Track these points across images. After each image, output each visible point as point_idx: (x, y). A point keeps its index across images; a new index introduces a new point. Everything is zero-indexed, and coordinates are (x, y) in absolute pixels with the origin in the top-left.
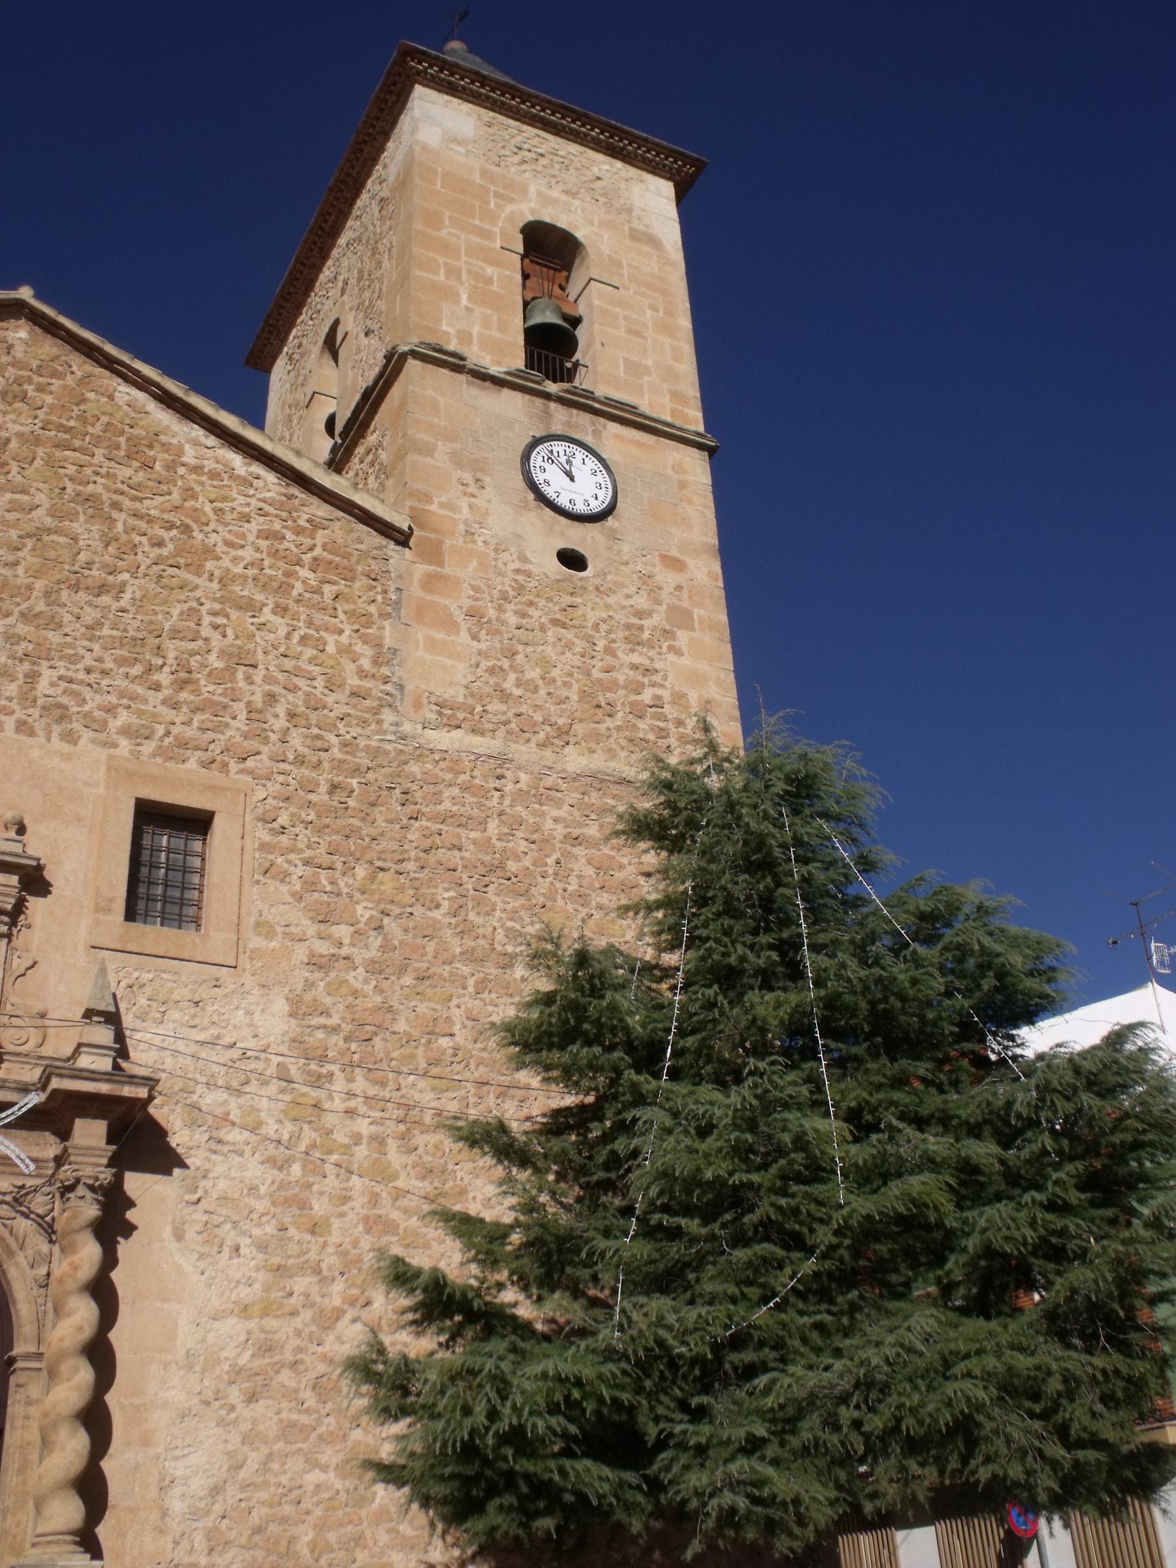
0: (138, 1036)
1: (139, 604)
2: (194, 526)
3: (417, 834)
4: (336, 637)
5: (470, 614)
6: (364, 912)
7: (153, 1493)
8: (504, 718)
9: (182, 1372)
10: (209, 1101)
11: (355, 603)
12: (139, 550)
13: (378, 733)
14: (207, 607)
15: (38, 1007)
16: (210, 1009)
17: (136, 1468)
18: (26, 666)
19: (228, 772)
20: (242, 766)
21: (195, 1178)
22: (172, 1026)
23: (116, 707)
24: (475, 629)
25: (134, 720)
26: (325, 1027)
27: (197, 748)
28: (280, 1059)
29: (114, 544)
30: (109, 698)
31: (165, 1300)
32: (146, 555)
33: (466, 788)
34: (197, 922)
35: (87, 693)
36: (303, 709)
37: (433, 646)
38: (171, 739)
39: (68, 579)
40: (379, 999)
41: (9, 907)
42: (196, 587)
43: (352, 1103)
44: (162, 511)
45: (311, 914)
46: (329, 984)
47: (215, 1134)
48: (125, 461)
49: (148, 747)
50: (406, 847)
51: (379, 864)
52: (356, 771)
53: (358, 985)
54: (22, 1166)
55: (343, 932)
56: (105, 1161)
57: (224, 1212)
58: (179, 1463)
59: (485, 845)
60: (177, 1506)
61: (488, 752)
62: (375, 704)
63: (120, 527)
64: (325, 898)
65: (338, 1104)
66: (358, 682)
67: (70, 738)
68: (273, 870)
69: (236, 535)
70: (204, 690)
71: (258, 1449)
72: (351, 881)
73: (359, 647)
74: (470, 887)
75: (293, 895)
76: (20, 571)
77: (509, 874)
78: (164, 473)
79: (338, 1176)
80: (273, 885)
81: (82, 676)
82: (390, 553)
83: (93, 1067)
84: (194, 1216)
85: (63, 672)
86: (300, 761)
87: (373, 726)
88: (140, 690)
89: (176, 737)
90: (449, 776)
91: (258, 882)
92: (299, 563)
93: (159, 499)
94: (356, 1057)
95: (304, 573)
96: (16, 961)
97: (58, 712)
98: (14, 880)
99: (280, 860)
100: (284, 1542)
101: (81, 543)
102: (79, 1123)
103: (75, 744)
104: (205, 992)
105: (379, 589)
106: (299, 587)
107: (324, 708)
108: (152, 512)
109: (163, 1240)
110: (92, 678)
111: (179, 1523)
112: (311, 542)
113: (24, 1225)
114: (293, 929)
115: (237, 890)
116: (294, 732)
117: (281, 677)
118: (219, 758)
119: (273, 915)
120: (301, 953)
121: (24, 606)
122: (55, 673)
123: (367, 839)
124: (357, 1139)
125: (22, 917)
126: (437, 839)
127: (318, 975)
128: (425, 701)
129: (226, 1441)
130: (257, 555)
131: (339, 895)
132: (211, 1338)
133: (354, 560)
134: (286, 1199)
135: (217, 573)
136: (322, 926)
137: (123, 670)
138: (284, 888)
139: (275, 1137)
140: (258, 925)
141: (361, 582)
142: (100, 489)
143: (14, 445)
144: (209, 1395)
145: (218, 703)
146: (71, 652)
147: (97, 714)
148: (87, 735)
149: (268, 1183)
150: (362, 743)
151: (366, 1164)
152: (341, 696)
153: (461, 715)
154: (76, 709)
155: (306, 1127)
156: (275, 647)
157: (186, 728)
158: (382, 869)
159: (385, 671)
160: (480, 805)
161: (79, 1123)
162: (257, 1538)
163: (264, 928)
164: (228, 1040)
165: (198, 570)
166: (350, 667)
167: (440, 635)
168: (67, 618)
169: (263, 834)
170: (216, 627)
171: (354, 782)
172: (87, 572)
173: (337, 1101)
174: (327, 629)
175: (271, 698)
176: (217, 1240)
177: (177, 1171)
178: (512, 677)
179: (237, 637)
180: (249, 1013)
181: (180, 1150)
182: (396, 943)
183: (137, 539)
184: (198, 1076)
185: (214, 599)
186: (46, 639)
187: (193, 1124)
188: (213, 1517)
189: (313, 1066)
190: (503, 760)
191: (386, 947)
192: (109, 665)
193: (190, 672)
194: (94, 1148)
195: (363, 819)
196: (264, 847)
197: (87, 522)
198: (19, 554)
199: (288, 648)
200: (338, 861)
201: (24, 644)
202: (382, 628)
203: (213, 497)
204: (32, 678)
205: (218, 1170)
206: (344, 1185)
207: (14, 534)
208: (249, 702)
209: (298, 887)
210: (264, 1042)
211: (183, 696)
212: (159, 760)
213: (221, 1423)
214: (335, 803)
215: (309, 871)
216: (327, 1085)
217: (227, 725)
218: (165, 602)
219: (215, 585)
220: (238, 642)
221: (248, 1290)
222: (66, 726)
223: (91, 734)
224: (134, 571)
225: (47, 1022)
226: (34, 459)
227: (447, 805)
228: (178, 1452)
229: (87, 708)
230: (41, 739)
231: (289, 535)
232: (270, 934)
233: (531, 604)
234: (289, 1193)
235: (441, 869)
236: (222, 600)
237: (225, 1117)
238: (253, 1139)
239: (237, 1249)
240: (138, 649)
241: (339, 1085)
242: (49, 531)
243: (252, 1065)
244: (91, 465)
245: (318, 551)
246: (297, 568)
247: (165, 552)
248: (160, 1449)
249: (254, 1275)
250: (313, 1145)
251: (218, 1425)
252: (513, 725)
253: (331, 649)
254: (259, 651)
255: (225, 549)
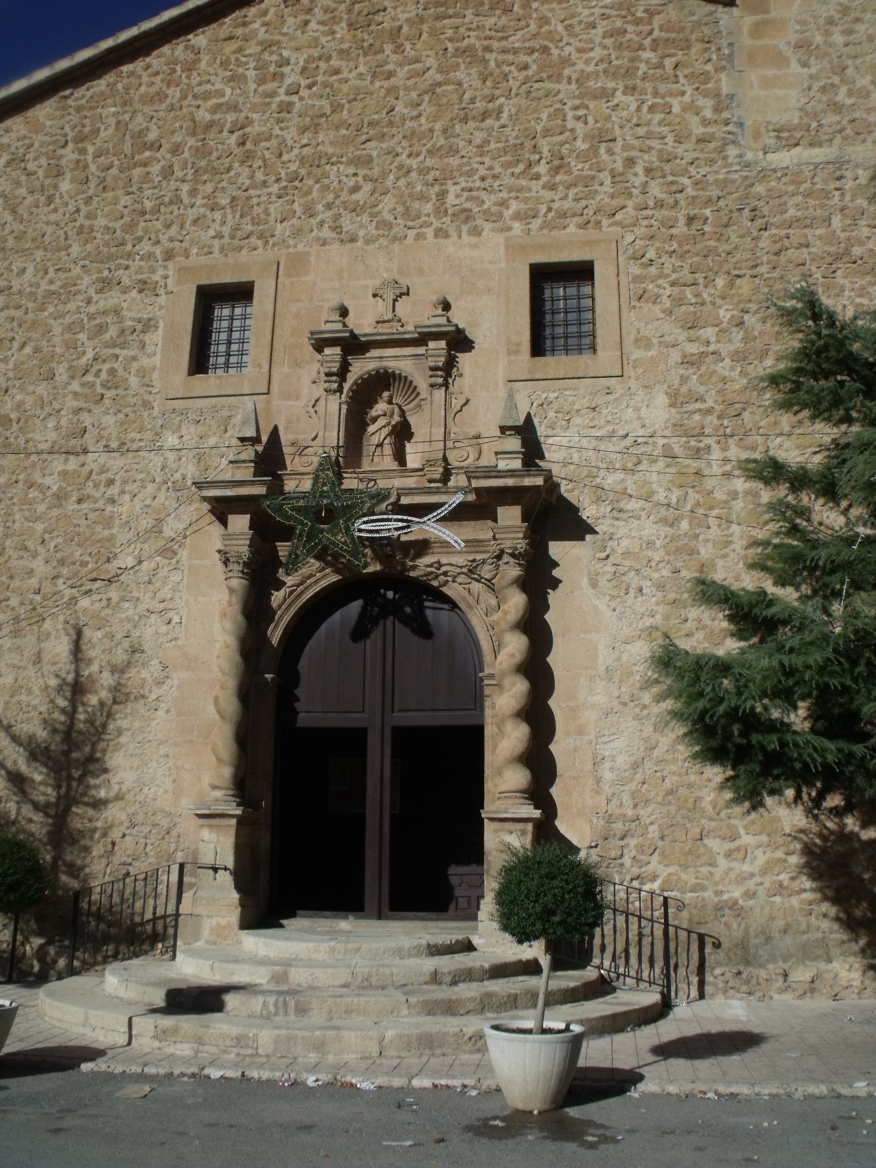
0: (550, 441)
1: (514, 118)
2: (551, 45)
3: (767, 242)
4: (680, 98)
5: (798, 46)
6: (725, 313)
7: (589, 766)
8: (839, 127)
9: (604, 683)
10: (609, 481)
11: (692, 66)
12: (510, 78)
13: (724, 167)
14: (569, 104)
15: (473, 432)
16: (604, 412)
17: (575, 750)
18: (437, 188)
19: (601, 228)
20: (612, 220)
21: (603, 540)
22: (576, 429)
23: (507, 200)
24: (804, 58)
25: (522, 206)
26: (700, 410)
27: (574, 215)
28: (665, 441)
29: (490, 79)
30: (501, 195)
31: (587, 632)
32: (516, 78)
33: (808, 195)
34: (593, 348)
35: (484, 196)
36: (657, 164)
37: (766, 83)
38: (553, 213)
39: (458, 115)
40: (745, 381)
41: (441, 364)
42: (559, 92)
43: (728, 467)
44: (524, 42)
45: (681, 324)
46: (701, 375)
47: (616, 506)
48: (489, 13)
49: (535, 224)
50: (758, 254)
51: (736, 272)
52: (709, 202)
53: (726, 373)
54: (456, 545)
55: (709, 333)
56: (521, 535)
57: (628, 563)
58: (607, 746)
59: (831, 238)
60: (608, 776)
61: (825, 159)
62: (719, 144)
63: (492, 64)
64: (692, 309)
65: (716, 469)
66: (703, 130)
67: (476, 231)
68: (646, 295)
69: (586, 42)
70: (574, 169)
71: (667, 736)
72: (712, 291)
73: (701, 102)
74: (819, 276)
75: (664, 312)
76: (423, 120)
77: (854, 258)
78: (521, 11)
79: (719, 526)
80: (646, 307)
81: (478, 184)
82: (719, 15)
83: (508, 467)
84: (605, 569)
85: (463, 185)
86: (660, 205)
87: (720, 163)
88: (523, 182)
89: (556, 211)
90: (791, 188)
91: (634, 307)
92: (641, 48)
93: (520, 33)
94: (728, 431)
95: (647, 55)
96: (454, 401)
97: (464, 215)
98: (443, 344)
99: (651, 286)
100: (691, 801)
101: (465, 86)
102: (501, 511)
103: (480, 235)
104: (600, 400)
105: (713, 49)
106: (643, 67)
107: (676, 158)
108: (516, 45)
109: (582, 589)
110: (486, 184)
111: (610, 787)
112: (648, 28)
113: (476, 587)
114: (667, 338)
115: (617, 317)
116: (652, 184)
117: (636, 143)
118: (593, 219)
119: (648, 331)
120: (675, 356)
121: (428, 146)
122: (458, 188)
123: (723, 255)
124: (734, 495)
125: (455, 369)
126: (786, 243)
127: (691, 371)
128: (763, 130)
129: (641, 730)
130: (605, 52)
131: (703, 304)
132: (624, 658)
133: (688, 31)
134: (677, 549)
135: (574, 76)
136: (692, 332)
137: (509, 171)
138: (656, 308)
139: (665, 502)
140: (637, 340)
141: (697, 48)
142: (473, 40)
143: (405, 29)
144: (626, 698)
145: (586, 177)
146: (468, 168)
147: (494, 209)
148: (487, 226)
149: (662, 538)
150: (711, 178)
151: (743, 515)
152: (689, 145)
153: (798, 135)
154: (477, 210)
155: (690, 491)
156: (628, 121)
157: (564, 202)
158: (739, 276)
159: (726, 115)
160: (822, 206)
161: (501, 511)
162: (670, 797)
163: (642, 342)
164: (621, 433)
165: (559, 78)
166: (694, 120)
167: (771, 72)
168: (462, 144)
169: (635, 269)
170: (578, 118)
171: (707, 212)
172: (471, 106)
173: (715, 467)
174: (671, 95)
175: (630, 162)
176: (623, 585)
177: (588, 537)
178: (844, 89)
179: (596, 121)
180: (637, 409)
181: (589, 521)
182: (756, 333)
183: (506, 69)
184: (600, 464)
185: (574, 97)
186: (448, 164)
187: (598, 500)
188: (635, 783)
189: (693, 443)
190: (839, 164)
191: (746, 340)
192: (498, 170)
193: (562, 158)
194: (512, 527)
195: (718, 240)
196: (636, 279)
197: (466, 68)
198: (421, 108)
199: (639, 118)
200: (700, 277)
201: (432, 173)
202: (720, 80)
203: (562, 17)
204: (442, 195)
205: (621, 532)
206: (725, 533)
207: (414, 95)
208: (612, 169)
209: (668, 305)
210: (651, 430)
211: (559, 178)
212: (545, 232)
213: (636, 717)
214: (693, 232)
215: (676, 290)
216: (706, 456)
217: (596, 192)
218: (535, 111)
219: (574, 86)
220: (598, 125)
221: (651, 620)
222: (472, 224)
223: (491, 225)
224: (508, 95)
225: (480, 441)
226: (421, 35)
227: (792, 212)
228: (606, 739)
229: (485, 207)
230: (454, 237)
231: (630, 28)
232: (649, 346)
233: (857, 20)
234: (679, 544)
235: (791, 267)
236: (581, 96)
237: (624, 492)
238: (647, 505)
239: (641, 590)
240: (519, 152)
241: (716, 454)
242: (439, 84)
243: (642, 450)
244: (464, 24)
245: (656, 34)
246: (640, 52)
247: (530, 72)
248: (592, 737)
249: (655, 608)
250: (698, 504)
251: (634, 719)
252: (848, 131)
253: (676, 109)
254: (616, 127)
255: (578, 55)
